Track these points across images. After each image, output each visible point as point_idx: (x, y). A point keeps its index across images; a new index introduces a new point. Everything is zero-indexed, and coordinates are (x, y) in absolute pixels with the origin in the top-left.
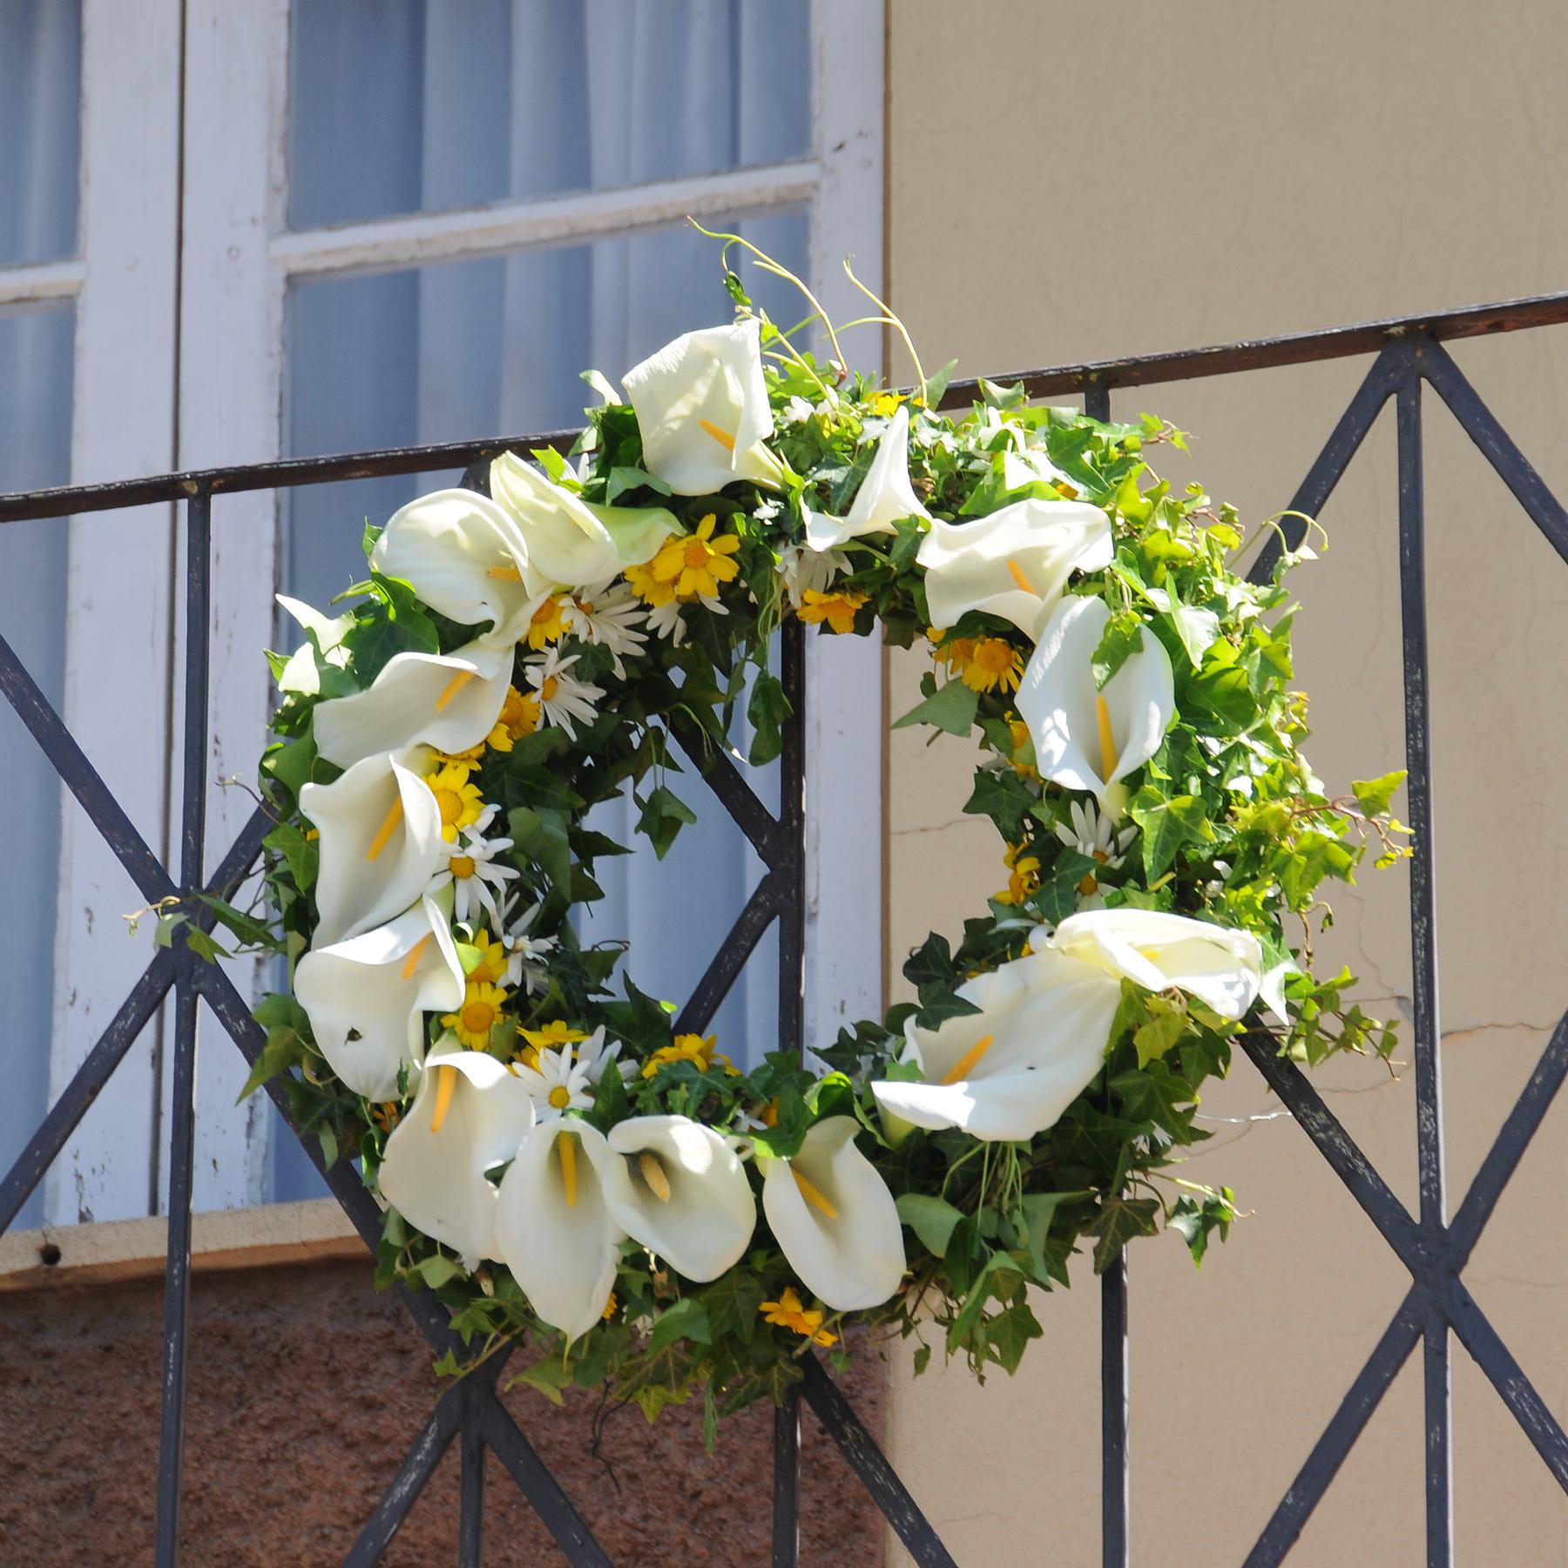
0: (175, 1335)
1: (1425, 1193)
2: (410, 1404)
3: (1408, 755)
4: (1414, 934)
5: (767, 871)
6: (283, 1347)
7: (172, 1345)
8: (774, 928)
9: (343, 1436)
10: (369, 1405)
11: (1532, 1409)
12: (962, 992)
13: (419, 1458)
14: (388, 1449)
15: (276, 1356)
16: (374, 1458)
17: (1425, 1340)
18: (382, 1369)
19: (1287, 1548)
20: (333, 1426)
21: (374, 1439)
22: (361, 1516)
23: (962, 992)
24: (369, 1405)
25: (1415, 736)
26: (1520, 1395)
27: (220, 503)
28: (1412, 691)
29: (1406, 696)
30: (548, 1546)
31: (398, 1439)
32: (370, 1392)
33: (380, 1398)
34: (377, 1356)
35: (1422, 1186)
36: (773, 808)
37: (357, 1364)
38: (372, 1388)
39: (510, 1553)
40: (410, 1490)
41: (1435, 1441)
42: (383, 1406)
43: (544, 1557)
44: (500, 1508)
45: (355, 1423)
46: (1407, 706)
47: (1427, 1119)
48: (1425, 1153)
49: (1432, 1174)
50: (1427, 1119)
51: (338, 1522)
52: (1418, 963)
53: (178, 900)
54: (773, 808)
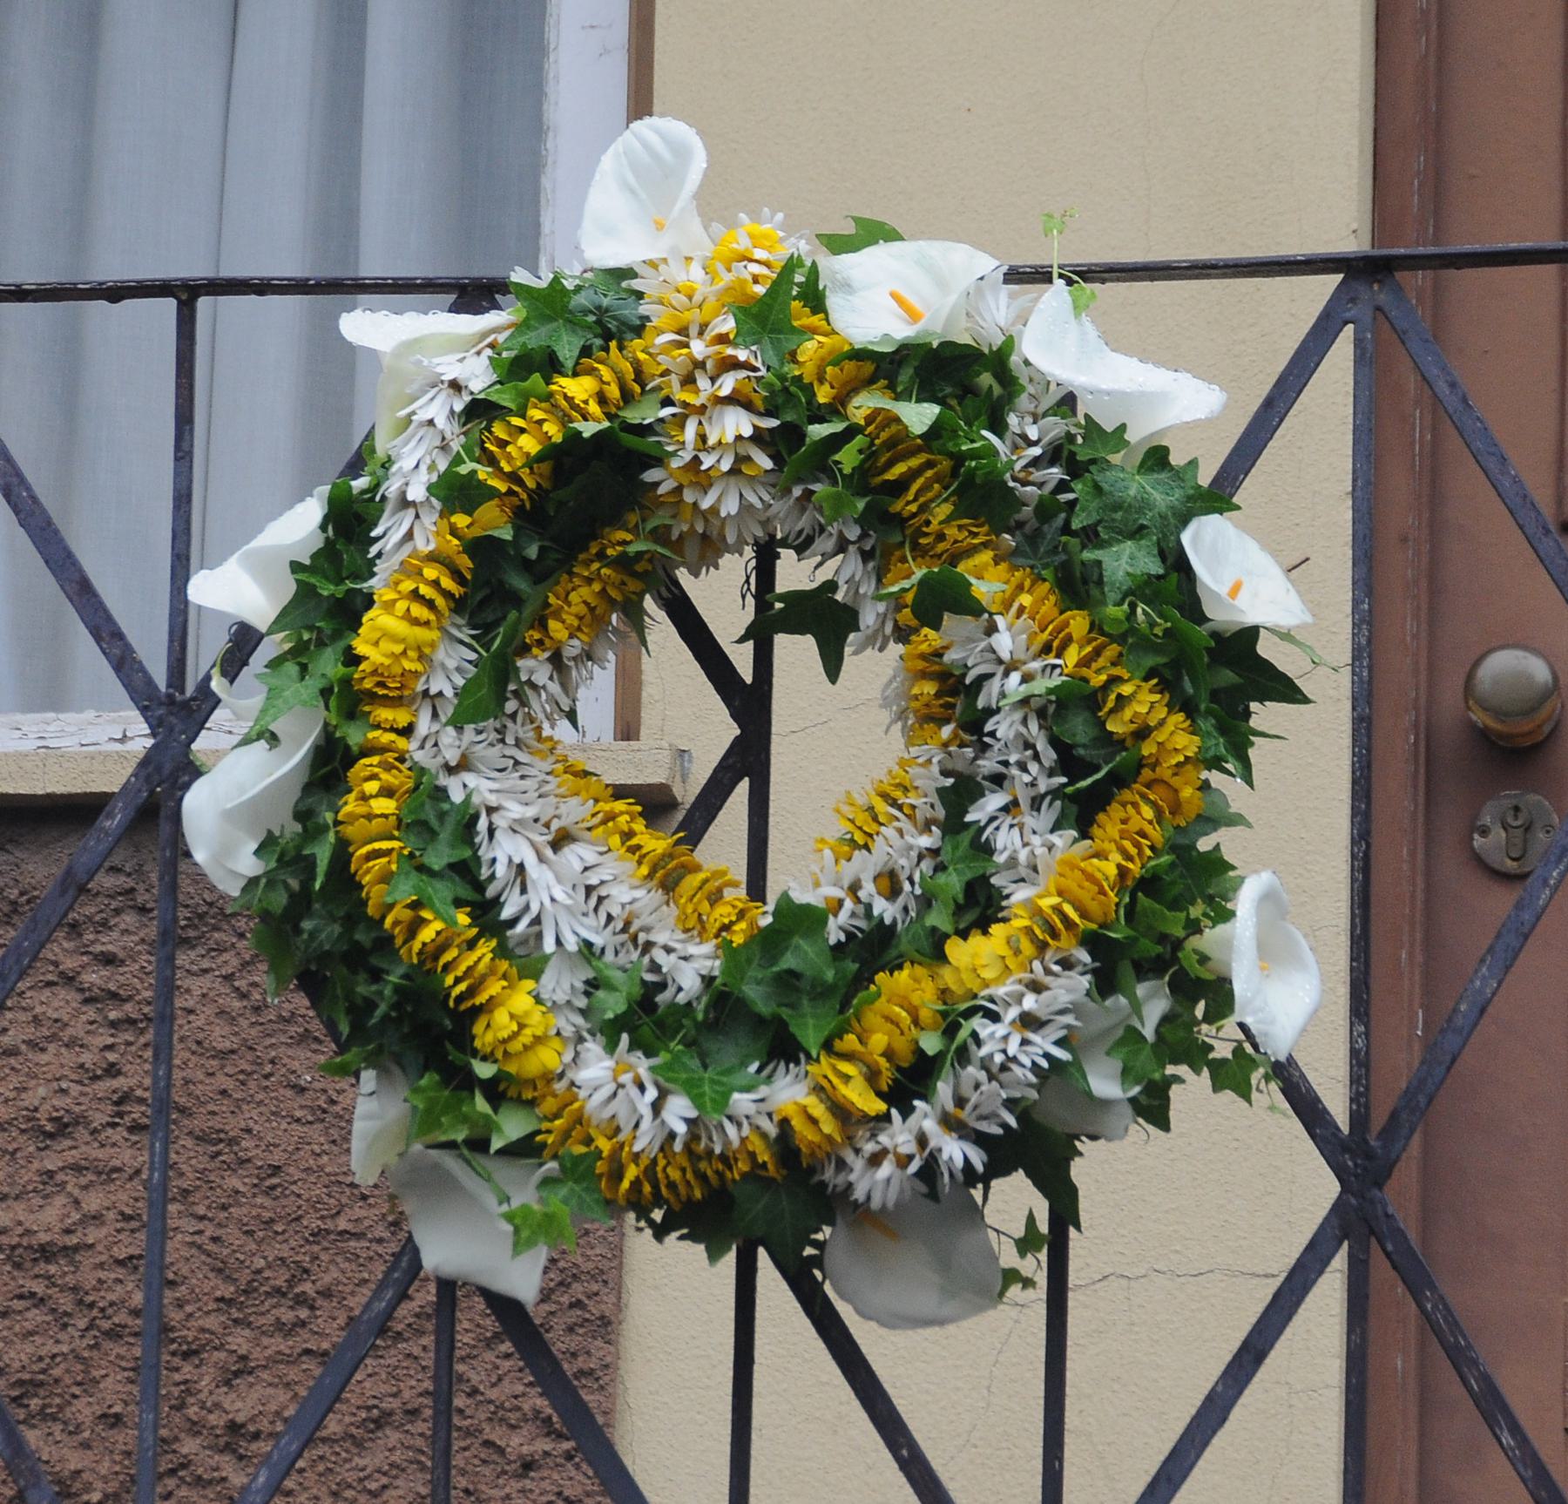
0: (160, 1134)
1: (1354, 1107)
2: (149, 962)
3: (1353, 683)
4: (1353, 857)
5: (738, 732)
6: (22, 894)
7: (157, 1145)
8: (744, 786)
9: (82, 990)
10: (109, 960)
11: (1445, 1320)
12: (750, 644)
13: (396, 1275)
14: (128, 1007)
15: (14, 903)
16: (113, 1015)
17: (1350, 1247)
18: (123, 926)
19: (1214, 1432)
20: (72, 979)
21: (114, 996)
22: (99, 1072)
23: (750, 644)
24: (109, 960)
25: (1361, 663)
26: (1435, 1306)
27: (204, 304)
28: (1359, 620)
29: (1354, 624)
30: (289, 1120)
31: (137, 998)
32: (110, 948)
33: (121, 955)
34: (117, 912)
35: (1352, 1100)
36: (746, 673)
37: (97, 918)
38: (109, 943)
39: (251, 1123)
40: (387, 1306)
41: (1356, 1344)
42: (122, 962)
43: (286, 1130)
44: (241, 1077)
45: (94, 977)
46: (1353, 634)
47: (1359, 1036)
48: (1355, 1069)
49: (1362, 1089)
50: (1359, 1036)
51: (74, 1077)
52: (1356, 886)
53: (450, 1027)
54: (746, 673)
